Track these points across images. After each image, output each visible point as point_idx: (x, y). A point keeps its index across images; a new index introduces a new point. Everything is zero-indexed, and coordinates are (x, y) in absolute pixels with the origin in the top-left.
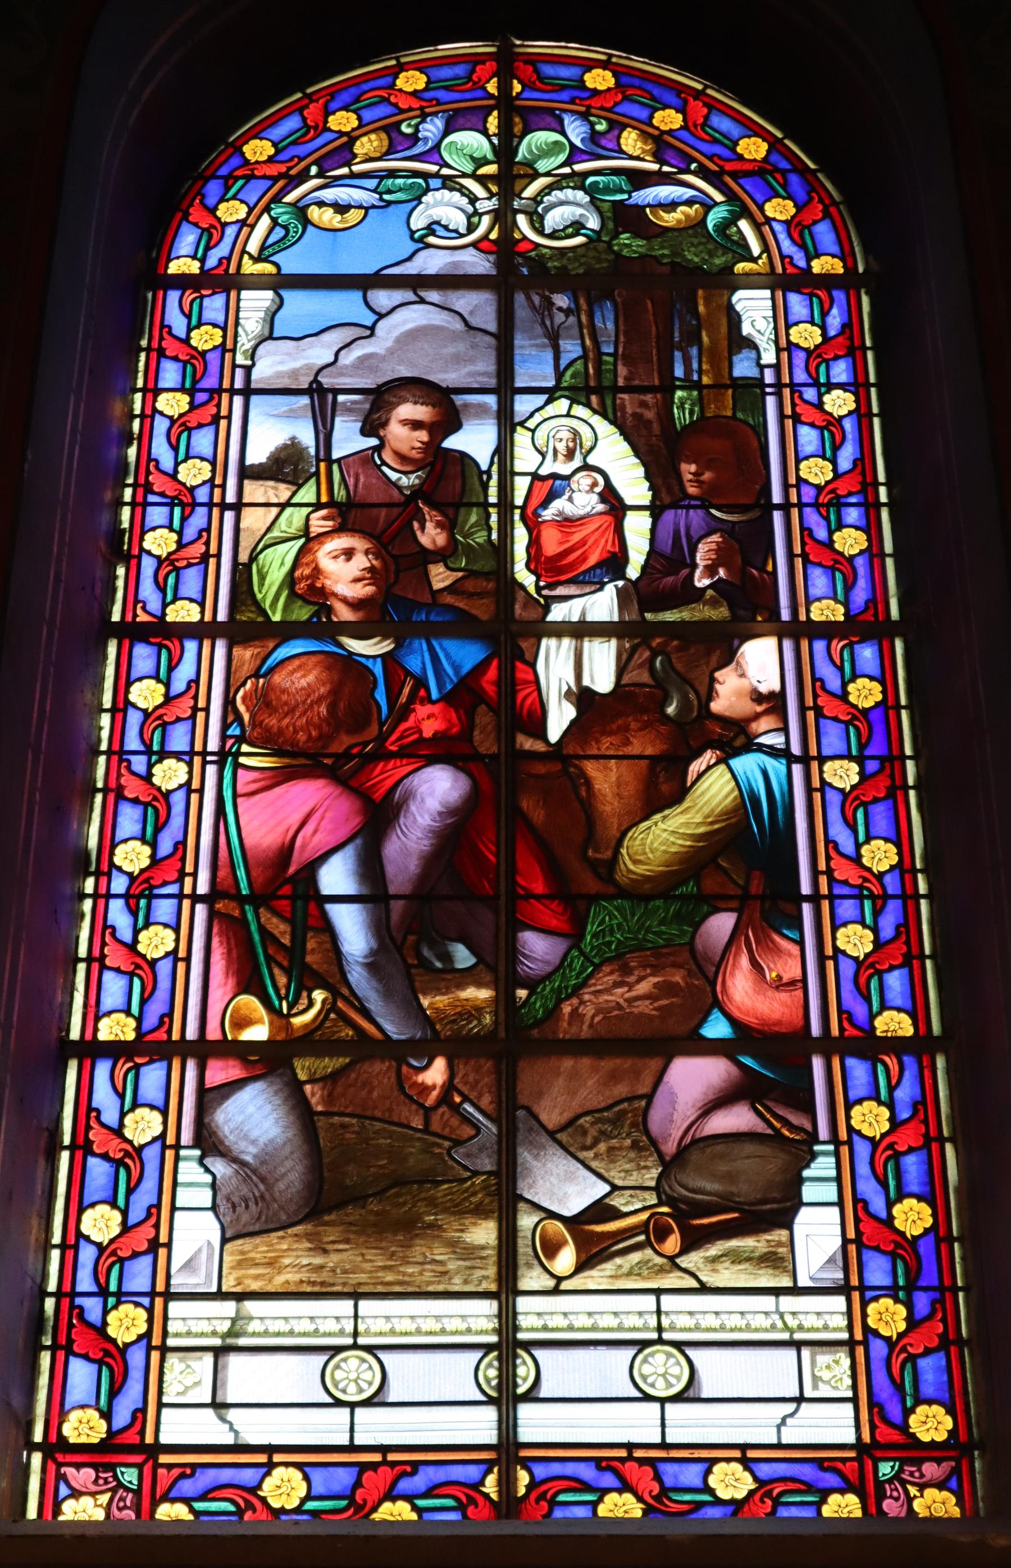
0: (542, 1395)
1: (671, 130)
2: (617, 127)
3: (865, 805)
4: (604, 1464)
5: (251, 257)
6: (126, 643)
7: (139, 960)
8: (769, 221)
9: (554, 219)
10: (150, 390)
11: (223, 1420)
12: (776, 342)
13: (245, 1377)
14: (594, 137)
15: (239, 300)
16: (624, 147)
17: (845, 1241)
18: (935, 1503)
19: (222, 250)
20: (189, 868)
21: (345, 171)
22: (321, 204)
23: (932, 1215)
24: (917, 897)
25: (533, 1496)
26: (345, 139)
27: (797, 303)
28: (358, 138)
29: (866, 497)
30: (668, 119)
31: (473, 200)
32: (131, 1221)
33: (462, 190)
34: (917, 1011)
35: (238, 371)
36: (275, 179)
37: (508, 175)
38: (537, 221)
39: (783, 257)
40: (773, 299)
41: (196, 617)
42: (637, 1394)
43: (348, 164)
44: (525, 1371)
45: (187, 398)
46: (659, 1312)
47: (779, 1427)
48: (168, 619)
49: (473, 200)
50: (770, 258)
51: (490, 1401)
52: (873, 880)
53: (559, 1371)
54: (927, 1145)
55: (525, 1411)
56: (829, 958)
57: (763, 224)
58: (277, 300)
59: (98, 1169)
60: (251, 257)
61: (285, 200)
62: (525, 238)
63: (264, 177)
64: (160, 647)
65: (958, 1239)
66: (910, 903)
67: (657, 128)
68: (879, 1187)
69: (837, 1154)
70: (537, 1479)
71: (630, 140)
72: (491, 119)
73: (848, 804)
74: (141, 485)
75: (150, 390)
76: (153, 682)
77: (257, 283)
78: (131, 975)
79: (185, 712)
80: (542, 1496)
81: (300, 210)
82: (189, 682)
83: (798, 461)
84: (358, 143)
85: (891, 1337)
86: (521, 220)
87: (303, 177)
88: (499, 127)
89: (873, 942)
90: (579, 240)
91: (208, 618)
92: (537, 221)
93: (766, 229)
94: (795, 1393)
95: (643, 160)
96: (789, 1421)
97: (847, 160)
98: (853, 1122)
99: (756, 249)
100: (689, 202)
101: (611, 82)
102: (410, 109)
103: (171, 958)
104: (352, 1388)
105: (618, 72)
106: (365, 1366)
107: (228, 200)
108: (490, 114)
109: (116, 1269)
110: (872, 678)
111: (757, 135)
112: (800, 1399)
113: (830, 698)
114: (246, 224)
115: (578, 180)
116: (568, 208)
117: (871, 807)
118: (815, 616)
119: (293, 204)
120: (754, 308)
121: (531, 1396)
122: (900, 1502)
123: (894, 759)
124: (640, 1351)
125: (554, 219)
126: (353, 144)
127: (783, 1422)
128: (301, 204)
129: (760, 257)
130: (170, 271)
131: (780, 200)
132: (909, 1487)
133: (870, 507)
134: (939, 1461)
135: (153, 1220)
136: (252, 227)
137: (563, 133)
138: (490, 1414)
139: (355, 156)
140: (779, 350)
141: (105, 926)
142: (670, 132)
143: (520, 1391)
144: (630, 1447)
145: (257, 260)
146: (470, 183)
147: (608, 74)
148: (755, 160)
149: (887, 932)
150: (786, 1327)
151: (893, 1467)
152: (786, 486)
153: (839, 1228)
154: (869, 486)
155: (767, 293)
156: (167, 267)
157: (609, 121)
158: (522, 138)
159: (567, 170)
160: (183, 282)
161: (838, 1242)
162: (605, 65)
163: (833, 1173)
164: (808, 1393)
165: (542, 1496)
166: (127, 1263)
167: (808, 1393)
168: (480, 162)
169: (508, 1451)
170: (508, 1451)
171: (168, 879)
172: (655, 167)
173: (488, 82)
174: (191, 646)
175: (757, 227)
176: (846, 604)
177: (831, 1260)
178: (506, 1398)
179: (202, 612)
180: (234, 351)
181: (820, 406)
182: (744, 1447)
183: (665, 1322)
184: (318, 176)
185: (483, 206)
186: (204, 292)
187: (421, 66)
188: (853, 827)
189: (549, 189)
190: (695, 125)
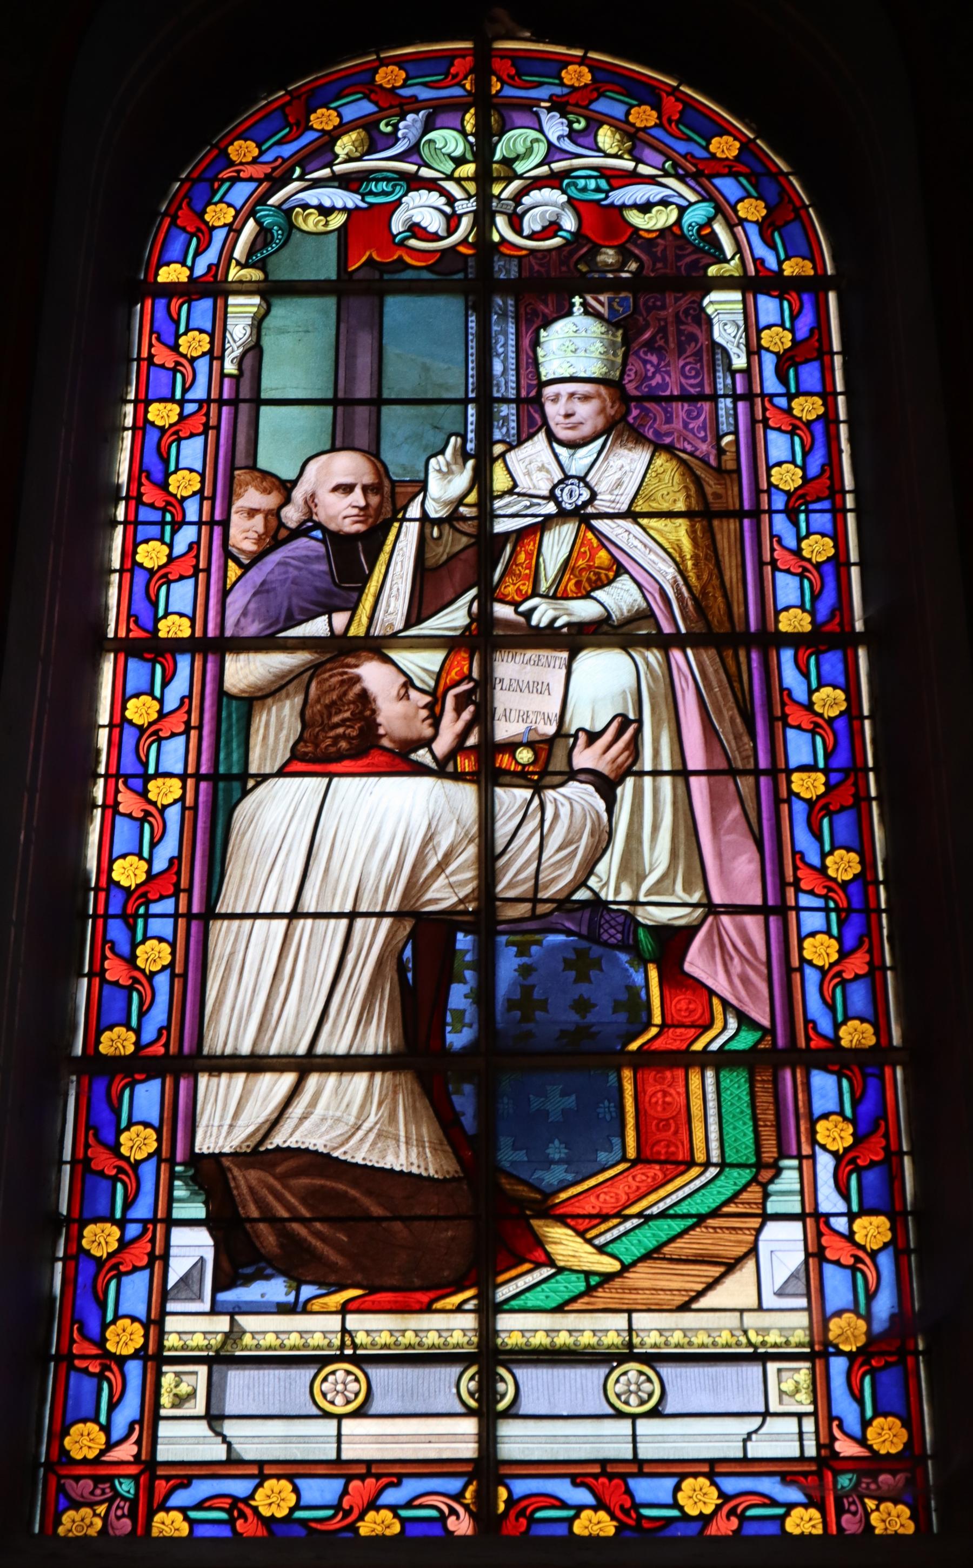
0: (522, 1412)
1: (646, 128)
2: (595, 123)
3: (830, 814)
4: (578, 1481)
5: (238, 263)
6: (122, 658)
7: (137, 974)
8: (742, 221)
9: (532, 223)
10: (141, 401)
11: (218, 1434)
12: (747, 345)
13: (242, 1388)
14: (572, 135)
15: (226, 306)
16: (601, 145)
17: (808, 1255)
18: (892, 1519)
19: (211, 256)
20: (184, 884)
21: (325, 172)
22: (305, 206)
23: (860, 863)
24: (845, 511)
25: (512, 1514)
26: (326, 138)
27: (768, 308)
28: (339, 138)
29: (833, 503)
30: (644, 116)
31: (451, 201)
32: (167, 709)
33: (444, 192)
34: (879, 1022)
35: (226, 381)
36: (260, 181)
37: (487, 168)
38: (516, 223)
39: (755, 260)
40: (744, 301)
41: (186, 633)
42: (610, 1411)
43: (330, 165)
44: (507, 1388)
45: (176, 409)
46: (630, 1330)
47: (745, 1441)
48: (162, 634)
49: (451, 201)
50: (742, 259)
51: (470, 1412)
52: (868, 1260)
53: (536, 1386)
54: (870, 974)
55: (507, 1429)
56: (764, 491)
57: (737, 225)
58: (265, 306)
59: (124, 828)
60: (238, 263)
61: (270, 202)
62: (503, 240)
63: (251, 179)
64: (154, 662)
65: (931, 1457)
66: (839, 516)
67: (633, 125)
68: (827, 1011)
69: (800, 1169)
70: (515, 1497)
71: (606, 138)
72: (468, 116)
73: (856, 1368)
74: (133, 498)
75: (141, 401)
76: (158, 543)
77: (243, 289)
78: (142, 821)
79: (141, 1260)
80: (522, 1513)
81: (286, 212)
82: (182, 699)
83: (769, 469)
84: (339, 143)
85: (838, 1151)
86: (501, 221)
87: (286, 180)
88: (476, 125)
89: (838, 952)
90: (556, 242)
91: (198, 634)
92: (516, 223)
93: (739, 230)
94: (762, 1409)
95: (621, 157)
96: (754, 1437)
97: (816, 154)
98: (773, 479)
99: (729, 250)
100: (664, 203)
101: (587, 78)
102: (391, 107)
103: (198, 497)
104: (339, 1400)
105: (594, 67)
106: (351, 1378)
107: (216, 204)
108: (467, 111)
109: (164, 589)
110: (863, 1020)
111: (729, 134)
112: (766, 1414)
113: (777, 412)
114: (234, 230)
115: (554, 180)
116: (546, 204)
117: (836, 817)
118: (783, 627)
119: (279, 207)
120: (724, 308)
121: (511, 1414)
122: (858, 1516)
123: (856, 770)
124: (613, 1369)
125: (532, 223)
126: (334, 144)
127: (749, 1435)
128: (285, 207)
129: (733, 258)
130: (160, 279)
131: (753, 200)
132: (867, 1501)
133: (838, 512)
134: (894, 1473)
135: (194, 553)
136: (239, 232)
137: (541, 131)
138: (470, 1426)
139: (337, 156)
140: (749, 354)
141: (105, 941)
142: (645, 129)
143: (502, 1406)
144: (604, 1463)
145: (243, 266)
146: (450, 186)
147: (585, 70)
148: (727, 159)
149: (814, 470)
150: (750, 1344)
151: (850, 1480)
152: (757, 491)
153: (802, 1244)
154: (836, 490)
155: (737, 296)
156: (157, 274)
157: (588, 119)
158: (501, 135)
159: (544, 170)
160: (171, 290)
161: (801, 1256)
162: (582, 61)
163: (797, 1187)
164: (772, 1409)
165: (522, 1513)
166: (164, 742)
167: (772, 1409)
168: (459, 161)
169: (487, 1468)
170: (487, 1468)
171: (164, 893)
172: (630, 165)
173: (465, 78)
174: (183, 663)
175: (731, 227)
176: (813, 613)
177: (793, 1276)
178: (488, 1412)
179: (193, 626)
180: (222, 358)
181: (789, 411)
182: (712, 1462)
183: (636, 1340)
184: (301, 178)
185: (461, 207)
186: (137, 1077)
187: (400, 62)
188: (818, 837)
189: (524, 191)
190: (670, 121)
